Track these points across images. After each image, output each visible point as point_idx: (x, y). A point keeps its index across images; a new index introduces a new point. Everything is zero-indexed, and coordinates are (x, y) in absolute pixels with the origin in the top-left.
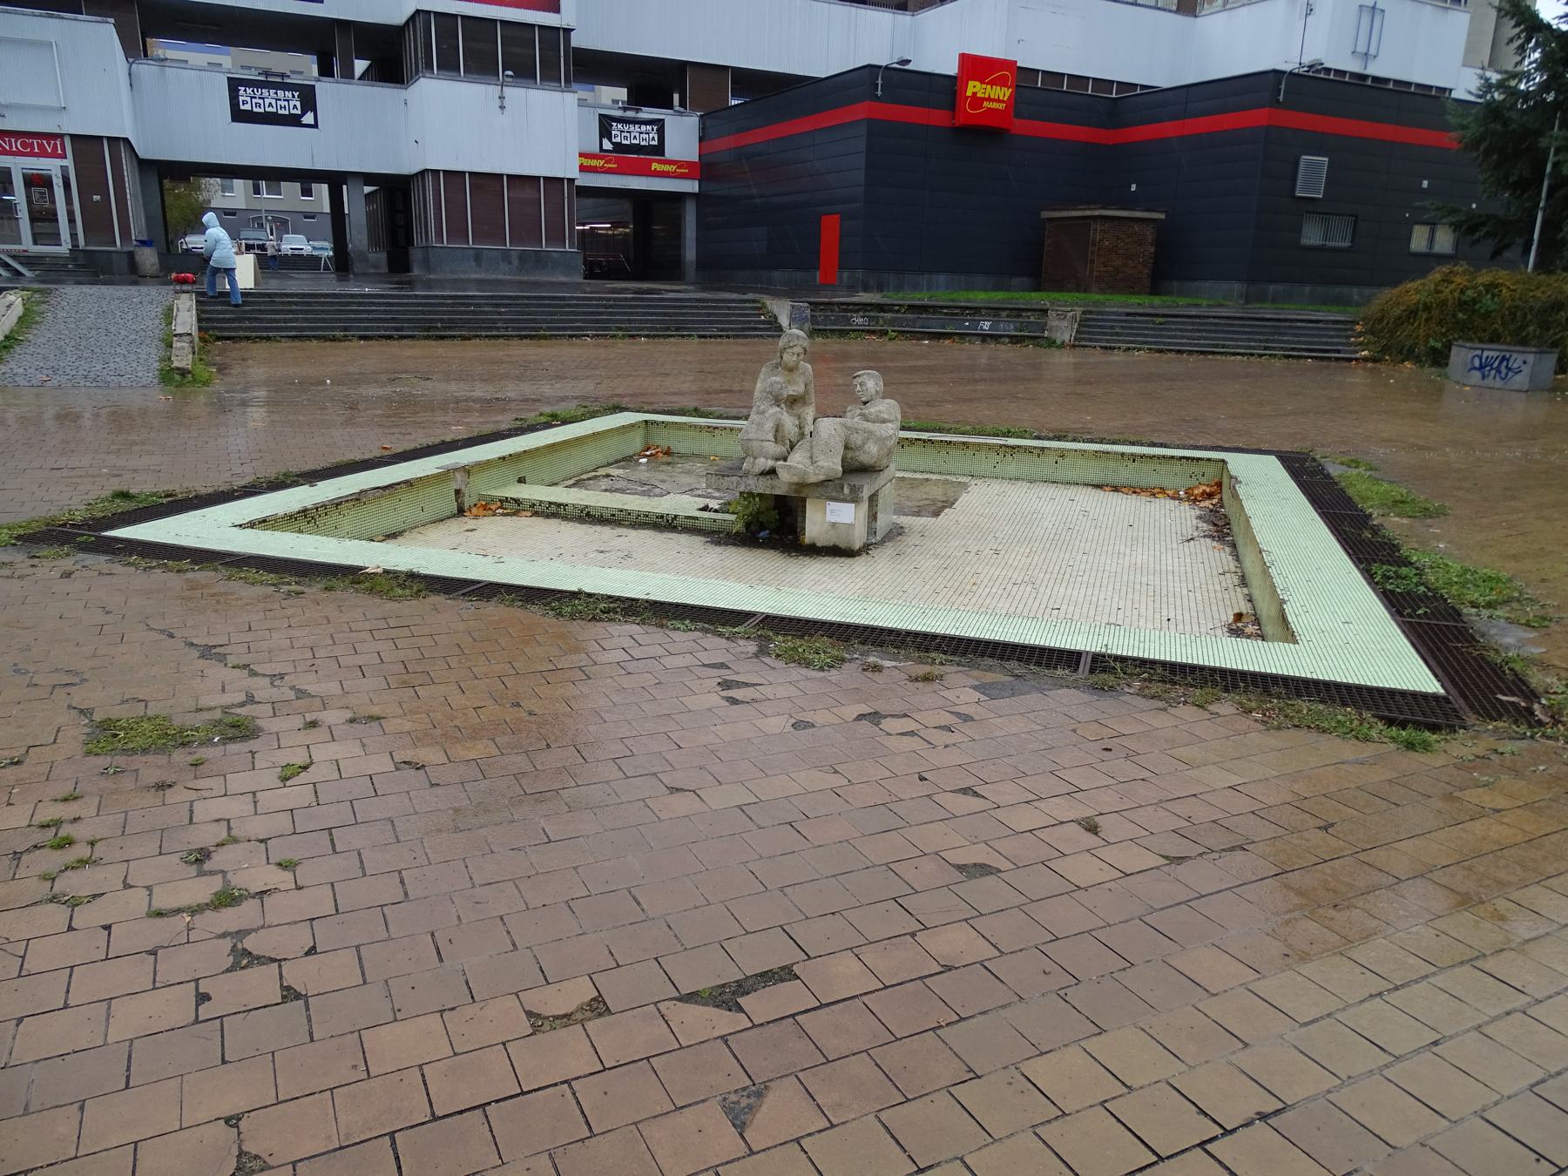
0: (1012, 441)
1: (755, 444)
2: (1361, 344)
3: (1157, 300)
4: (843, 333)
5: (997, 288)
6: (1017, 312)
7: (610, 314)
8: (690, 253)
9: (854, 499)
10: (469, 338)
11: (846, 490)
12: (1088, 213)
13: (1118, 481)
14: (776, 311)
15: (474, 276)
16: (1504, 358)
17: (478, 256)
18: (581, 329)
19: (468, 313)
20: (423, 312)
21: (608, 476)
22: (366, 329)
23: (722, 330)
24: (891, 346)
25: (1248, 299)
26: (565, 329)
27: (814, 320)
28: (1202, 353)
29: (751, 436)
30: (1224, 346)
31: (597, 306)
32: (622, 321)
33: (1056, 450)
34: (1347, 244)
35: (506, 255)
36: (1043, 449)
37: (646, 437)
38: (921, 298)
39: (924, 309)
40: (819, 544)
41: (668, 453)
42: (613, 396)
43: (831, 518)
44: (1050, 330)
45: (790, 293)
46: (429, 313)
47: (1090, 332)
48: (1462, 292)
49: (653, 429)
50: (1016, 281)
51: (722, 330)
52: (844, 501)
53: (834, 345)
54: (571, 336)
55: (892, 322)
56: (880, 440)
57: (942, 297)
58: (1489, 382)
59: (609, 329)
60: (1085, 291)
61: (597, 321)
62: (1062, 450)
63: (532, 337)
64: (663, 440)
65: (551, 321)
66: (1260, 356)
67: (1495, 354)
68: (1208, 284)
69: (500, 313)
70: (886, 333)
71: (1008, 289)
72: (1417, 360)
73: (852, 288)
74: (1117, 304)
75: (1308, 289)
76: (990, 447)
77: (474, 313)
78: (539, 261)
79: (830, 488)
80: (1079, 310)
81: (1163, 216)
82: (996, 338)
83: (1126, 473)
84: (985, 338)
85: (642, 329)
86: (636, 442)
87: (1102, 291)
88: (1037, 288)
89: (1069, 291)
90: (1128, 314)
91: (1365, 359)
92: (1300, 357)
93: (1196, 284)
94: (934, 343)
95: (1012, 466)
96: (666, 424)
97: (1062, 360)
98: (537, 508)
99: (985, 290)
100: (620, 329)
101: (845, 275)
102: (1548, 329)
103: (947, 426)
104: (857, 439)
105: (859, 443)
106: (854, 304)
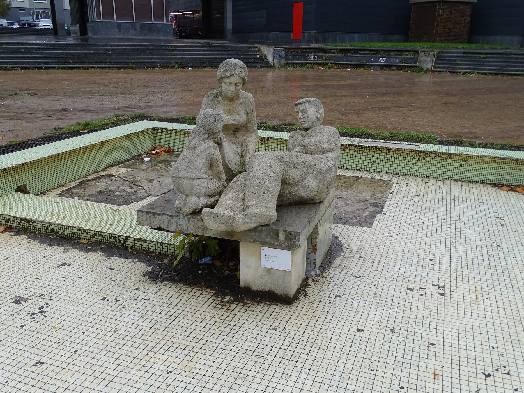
0: (424, 147)
3: (473, 46)
4: (303, 65)
5: (385, 41)
6: (400, 52)
7: (172, 54)
8: (229, 25)
9: (290, 244)
10: (87, 69)
11: (282, 237)
13: (513, 181)
14: (266, 53)
15: (117, 36)
17: (119, 26)
18: (154, 63)
19: (89, 54)
20: (63, 54)
21: (111, 176)
22: (27, 63)
24: (330, 72)
26: (144, 63)
27: (286, 57)
28: (510, 75)
31: (165, 50)
32: (179, 59)
35: (133, 25)
36: (450, 155)
37: (155, 139)
38: (347, 46)
39: (348, 51)
40: (254, 288)
43: (265, 263)
44: (420, 62)
45: (276, 43)
46: (67, 54)
47: (442, 63)
50: (395, 37)
52: (279, 247)
53: (298, 71)
54: (148, 67)
55: (330, 59)
56: (320, 174)
57: (357, 45)
59: (170, 63)
60: (433, 42)
61: (164, 59)
62: (466, 156)
63: (125, 68)
64: (166, 142)
65: (137, 59)
68: (499, 37)
69: (108, 54)
70: (327, 64)
71: (391, 41)
73: (309, 41)
74: (452, 47)
76: (407, 152)
77: (93, 54)
78: (151, 29)
79: (266, 234)
80: (436, 51)
82: (389, 67)
85: (189, 63)
86: (146, 144)
88: (407, 41)
89: (425, 42)
90: (464, 53)
94: (354, 70)
95: (424, 167)
96: (167, 131)
97: (427, 78)
98: (11, 223)
99: (379, 42)
100: (177, 63)
101: (306, 34)
103: (371, 132)
104: (295, 174)
105: (297, 178)
106: (310, 49)
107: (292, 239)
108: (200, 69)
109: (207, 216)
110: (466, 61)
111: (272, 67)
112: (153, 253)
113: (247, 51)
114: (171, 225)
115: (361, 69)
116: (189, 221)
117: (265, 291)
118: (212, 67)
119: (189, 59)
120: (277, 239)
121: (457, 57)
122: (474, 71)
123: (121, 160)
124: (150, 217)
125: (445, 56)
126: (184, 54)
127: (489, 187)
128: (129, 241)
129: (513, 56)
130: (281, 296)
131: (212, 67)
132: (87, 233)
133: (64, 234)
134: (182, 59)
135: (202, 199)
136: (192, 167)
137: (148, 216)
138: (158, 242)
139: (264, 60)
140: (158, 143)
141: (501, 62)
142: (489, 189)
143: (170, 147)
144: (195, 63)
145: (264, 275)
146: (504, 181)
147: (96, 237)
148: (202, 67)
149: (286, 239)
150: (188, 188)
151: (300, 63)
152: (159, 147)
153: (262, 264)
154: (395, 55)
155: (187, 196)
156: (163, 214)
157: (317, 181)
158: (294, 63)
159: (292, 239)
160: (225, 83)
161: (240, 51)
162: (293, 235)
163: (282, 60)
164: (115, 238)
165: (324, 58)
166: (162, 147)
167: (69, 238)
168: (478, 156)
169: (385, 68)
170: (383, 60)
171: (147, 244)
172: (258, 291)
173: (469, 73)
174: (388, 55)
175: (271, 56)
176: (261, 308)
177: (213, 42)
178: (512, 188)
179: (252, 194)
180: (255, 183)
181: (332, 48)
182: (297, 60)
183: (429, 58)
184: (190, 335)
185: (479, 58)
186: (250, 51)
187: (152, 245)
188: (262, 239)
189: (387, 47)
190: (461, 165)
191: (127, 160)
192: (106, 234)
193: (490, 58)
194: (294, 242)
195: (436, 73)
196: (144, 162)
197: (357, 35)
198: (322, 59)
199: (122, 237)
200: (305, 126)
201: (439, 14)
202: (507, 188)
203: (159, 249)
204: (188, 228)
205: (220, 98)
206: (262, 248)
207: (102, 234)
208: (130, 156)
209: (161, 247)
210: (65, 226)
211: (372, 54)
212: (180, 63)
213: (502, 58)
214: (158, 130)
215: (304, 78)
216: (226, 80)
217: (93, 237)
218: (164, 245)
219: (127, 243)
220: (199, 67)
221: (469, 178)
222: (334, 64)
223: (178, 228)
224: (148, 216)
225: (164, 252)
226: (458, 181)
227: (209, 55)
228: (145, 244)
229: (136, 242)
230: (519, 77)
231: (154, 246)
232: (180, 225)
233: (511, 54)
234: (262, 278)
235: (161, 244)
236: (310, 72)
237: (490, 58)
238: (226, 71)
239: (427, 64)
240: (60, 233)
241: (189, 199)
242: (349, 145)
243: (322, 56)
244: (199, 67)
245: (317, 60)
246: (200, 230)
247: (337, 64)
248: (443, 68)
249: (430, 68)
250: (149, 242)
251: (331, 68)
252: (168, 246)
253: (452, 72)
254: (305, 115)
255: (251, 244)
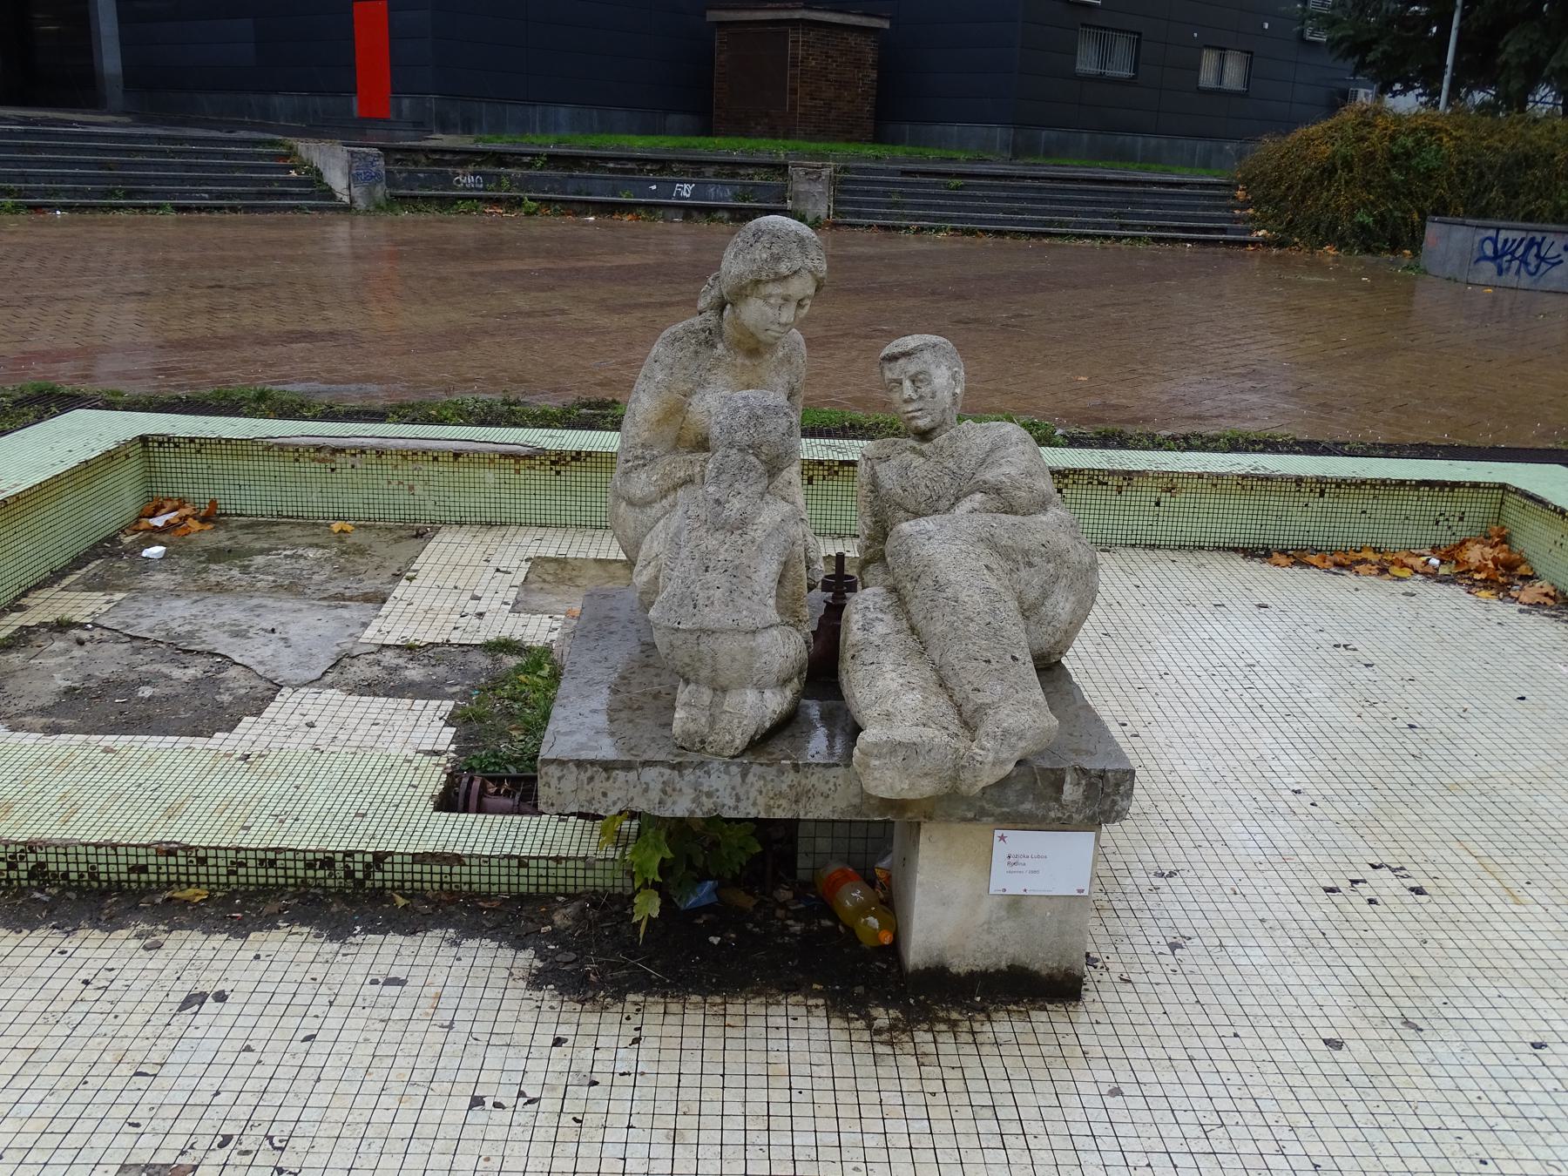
1: (728, 646)
2: (1252, 218)
4: (446, 203)
8: (111, 61)
12: (784, 15)
16: (1532, 242)
23: (220, 196)
25: (1017, 152)
28: (1033, 234)
29: (712, 617)
30: (1061, 224)
33: (1159, 475)
34: (1126, 73)
36: (1128, 475)
37: (149, 476)
39: (573, 161)
40: (959, 966)
41: (212, 516)
42: (28, 357)
43: (1005, 881)
44: (796, 198)
48: (1393, 139)
49: (166, 460)
50: (674, 119)
51: (220, 196)
55: (524, 184)
58: (1509, 279)
64: (197, 484)
66: (1119, 238)
67: (1518, 235)
68: (955, 129)
70: (519, 203)
72: (1341, 243)
73: (420, 126)
75: (1085, 137)
81: (886, 25)
82: (708, 211)
83: (1303, 522)
84: (688, 212)
85: (56, 193)
87: (810, 137)
88: (707, 131)
90: (904, 173)
91: (1266, 243)
92: (1175, 240)
93: (938, 128)
94: (606, 220)
96: (198, 444)
102: (1516, 195)
107: (1108, 795)
108: (99, 216)
109: (878, 757)
110: (916, 195)
111: (348, 209)
112: (488, 896)
113: (251, 156)
114: (675, 796)
115: (627, 218)
116: (744, 776)
117: (998, 971)
118: (143, 208)
119: (50, 178)
120: (1058, 800)
121: (887, 183)
122: (943, 224)
123: (60, 561)
124: (591, 779)
125: (855, 181)
126: (28, 163)
127: (1238, 557)
128: (388, 867)
129: (1029, 182)
130: (1050, 976)
131: (143, 208)
132: (202, 861)
133: (94, 876)
134: (25, 177)
135: (768, 694)
136: (748, 593)
137: (584, 777)
138: (509, 857)
139: (315, 186)
140: (162, 491)
141: (1007, 199)
142: (1238, 564)
143: (213, 503)
144: (75, 193)
145: (1000, 920)
146: (1269, 538)
147: (242, 871)
148: (102, 208)
149: (1087, 798)
150: (736, 665)
151: (439, 198)
152: (169, 505)
153: (996, 886)
154: (716, 176)
155: (721, 690)
156: (645, 764)
157: (1072, 599)
158: (415, 197)
159: (1108, 795)
160: (766, 298)
161: (226, 155)
162: (1112, 781)
163: (379, 188)
164: (328, 863)
165: (505, 182)
166: (182, 503)
167: (117, 887)
168: (1200, 476)
169: (695, 214)
170: (686, 190)
171: (466, 870)
172: (972, 974)
173: (931, 229)
174: (697, 174)
175: (339, 174)
176: (1003, 1026)
177: (101, 119)
178: (1298, 557)
179: (975, 663)
180: (973, 627)
181: (523, 149)
182: (423, 187)
183: (819, 188)
184: (19, 1124)
185: (947, 187)
186: (260, 156)
187: (485, 870)
188: (1006, 805)
189: (667, 150)
190: (1158, 504)
191: (78, 562)
192: (290, 855)
193: (973, 187)
194: (1114, 803)
195: (844, 232)
196: (148, 565)
197: (563, 112)
198: (499, 184)
199: (358, 857)
200: (923, 423)
201: (794, 57)
202: (1283, 560)
203: (514, 880)
204: (738, 799)
205: (720, 346)
206: (998, 833)
207: (271, 855)
208: (83, 546)
209: (523, 871)
210: (97, 846)
211: (650, 171)
212: (20, 193)
213: (1004, 188)
214: (161, 444)
215: (490, 248)
216: (775, 289)
217: (230, 873)
218: (533, 863)
219: (378, 875)
220: (93, 207)
221: (1180, 538)
222: (543, 200)
223: (700, 805)
224: (584, 777)
225: (532, 889)
226: (1153, 547)
227: (122, 165)
228: (456, 869)
229: (417, 868)
230: (1058, 242)
231: (495, 871)
232: (709, 795)
233: (1024, 178)
234: (989, 931)
235: (522, 862)
236: (463, 228)
237: (973, 187)
238: (777, 259)
239: (815, 205)
240: (73, 876)
241: (730, 701)
242: (842, 463)
243: (499, 175)
244: (93, 207)
245: (485, 189)
246: (784, 802)
247: (550, 200)
248: (858, 215)
249: (823, 216)
250: (475, 861)
251: (534, 213)
252: (552, 864)
253: (886, 228)
254: (925, 390)
255: (970, 826)
